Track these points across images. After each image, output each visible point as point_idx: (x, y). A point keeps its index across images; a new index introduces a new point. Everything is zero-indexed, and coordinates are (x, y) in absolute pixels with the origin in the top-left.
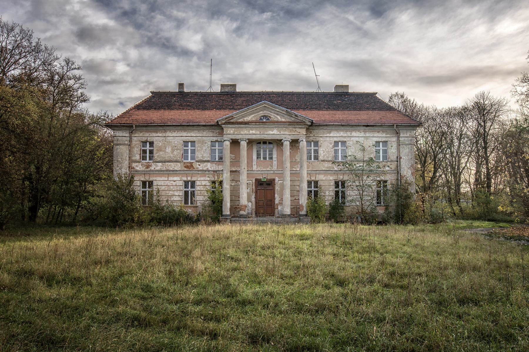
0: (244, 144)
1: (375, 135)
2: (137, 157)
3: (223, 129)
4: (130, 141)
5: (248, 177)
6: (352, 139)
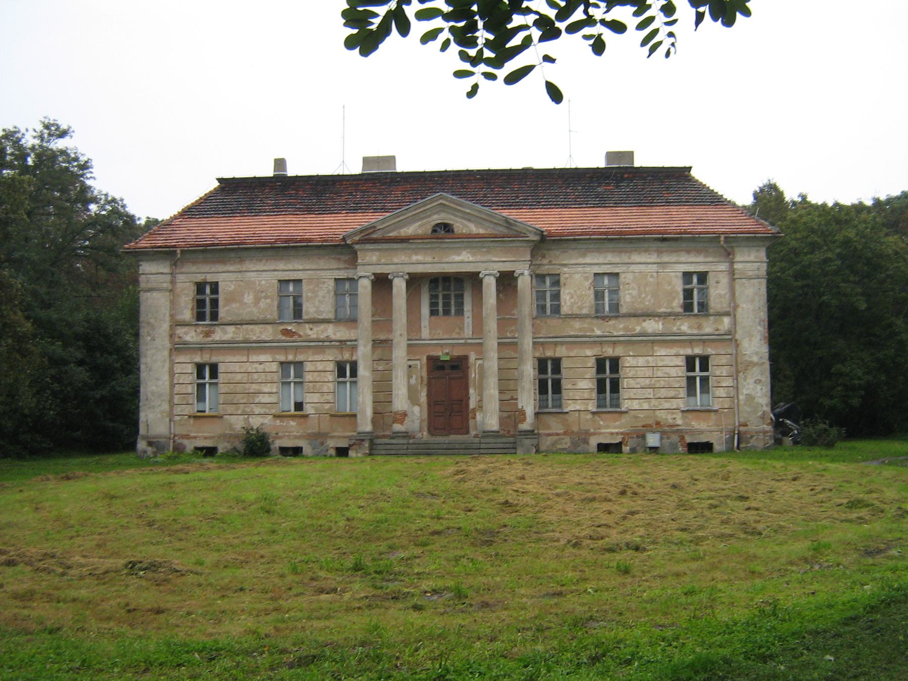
0: (399, 286)
1: (683, 259)
2: (187, 314)
3: (356, 253)
4: (173, 282)
5: (409, 353)
6: (633, 268)
